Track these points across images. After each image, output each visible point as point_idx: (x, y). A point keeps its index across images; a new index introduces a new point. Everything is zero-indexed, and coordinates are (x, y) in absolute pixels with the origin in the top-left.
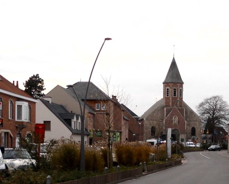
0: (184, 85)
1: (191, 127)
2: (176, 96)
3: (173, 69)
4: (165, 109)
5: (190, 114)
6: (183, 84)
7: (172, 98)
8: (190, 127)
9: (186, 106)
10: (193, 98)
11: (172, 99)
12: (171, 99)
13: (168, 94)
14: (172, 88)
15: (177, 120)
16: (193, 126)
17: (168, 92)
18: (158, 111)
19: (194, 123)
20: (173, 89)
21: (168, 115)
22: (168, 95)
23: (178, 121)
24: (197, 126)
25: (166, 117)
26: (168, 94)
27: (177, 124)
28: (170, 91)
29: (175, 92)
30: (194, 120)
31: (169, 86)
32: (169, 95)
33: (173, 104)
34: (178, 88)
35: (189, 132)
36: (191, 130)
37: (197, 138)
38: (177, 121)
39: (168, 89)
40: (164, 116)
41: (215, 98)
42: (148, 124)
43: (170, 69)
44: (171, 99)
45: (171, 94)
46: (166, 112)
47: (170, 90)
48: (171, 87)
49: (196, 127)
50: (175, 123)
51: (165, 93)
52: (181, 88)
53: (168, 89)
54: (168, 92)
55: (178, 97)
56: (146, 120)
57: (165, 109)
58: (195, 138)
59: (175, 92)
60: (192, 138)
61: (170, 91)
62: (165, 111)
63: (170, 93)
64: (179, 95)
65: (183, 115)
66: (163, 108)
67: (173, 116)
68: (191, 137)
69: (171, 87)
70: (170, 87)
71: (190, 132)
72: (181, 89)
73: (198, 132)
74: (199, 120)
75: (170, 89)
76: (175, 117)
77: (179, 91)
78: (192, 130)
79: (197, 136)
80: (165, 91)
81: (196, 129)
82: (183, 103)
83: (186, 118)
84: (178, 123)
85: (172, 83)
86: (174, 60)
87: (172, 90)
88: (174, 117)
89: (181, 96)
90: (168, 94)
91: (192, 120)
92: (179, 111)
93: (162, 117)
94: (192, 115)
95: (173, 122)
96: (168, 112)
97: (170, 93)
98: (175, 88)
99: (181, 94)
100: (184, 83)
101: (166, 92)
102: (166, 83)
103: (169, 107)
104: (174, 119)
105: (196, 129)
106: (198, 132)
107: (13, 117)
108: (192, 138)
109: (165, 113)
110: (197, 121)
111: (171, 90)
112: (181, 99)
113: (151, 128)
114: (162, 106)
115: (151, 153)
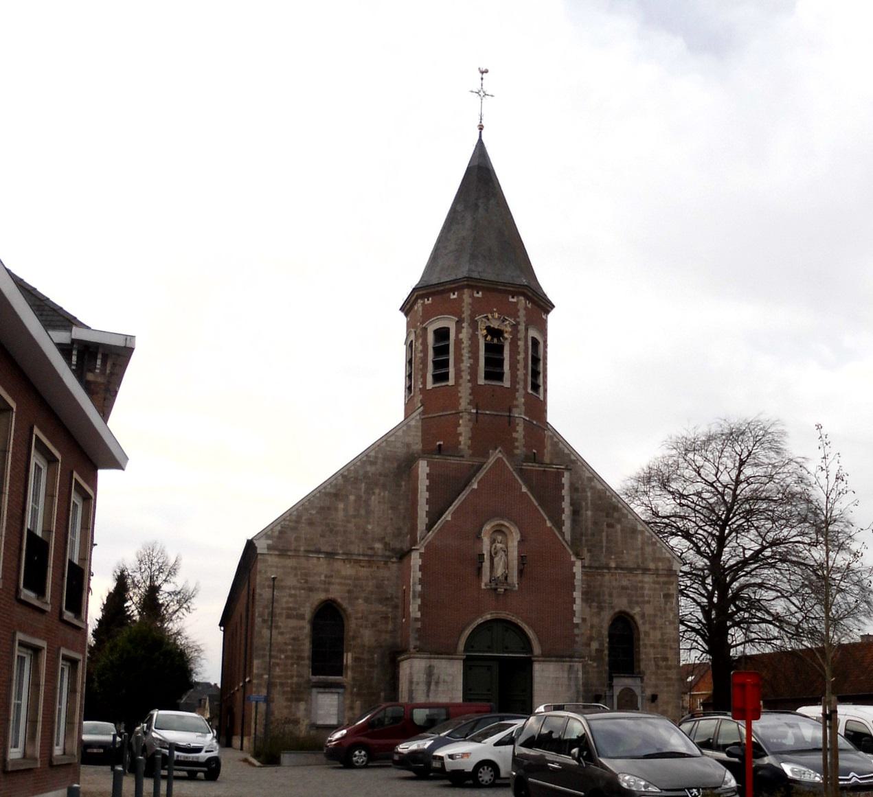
0: (552, 319)
1: (607, 616)
2: (507, 383)
3: (476, 206)
4: (423, 468)
5: (595, 523)
6: (547, 312)
7: (476, 390)
8: (601, 608)
9: (570, 461)
10: (619, 401)
11: (474, 403)
12: (464, 403)
13: (445, 364)
14: (474, 325)
15: (514, 553)
16: (621, 604)
17: (441, 350)
18: (370, 491)
19: (625, 582)
20: (482, 326)
21: (448, 516)
22: (445, 377)
23: (522, 559)
24: (649, 609)
25: (429, 527)
26: (441, 364)
27: (514, 578)
28: (458, 342)
29: (494, 350)
30: (630, 559)
31: (456, 311)
32: (452, 370)
33: (481, 446)
34: (515, 327)
35: (595, 645)
36: (605, 632)
37: (649, 692)
38: (514, 563)
39: (442, 334)
40: (414, 528)
41: (733, 436)
42: (291, 581)
43: (459, 208)
44: (464, 403)
45: (466, 364)
46: (429, 489)
47: (460, 336)
48: (466, 315)
49: (643, 616)
50: (499, 572)
51: (424, 361)
52: (533, 333)
53: (442, 334)
54: (441, 350)
55: (520, 386)
56: (269, 548)
57: (423, 468)
58: (638, 691)
59: (494, 350)
60: (617, 691)
61: (458, 342)
62: (423, 483)
63: (458, 360)
64: (523, 373)
65: (559, 524)
66: (406, 467)
67: (488, 519)
68: (611, 686)
69: (466, 315)
70: (457, 313)
71: (599, 651)
72: (535, 343)
73: (653, 646)
74: (656, 560)
75: (458, 331)
76: (499, 530)
77: (521, 343)
78: (611, 636)
79: (650, 679)
80: (425, 351)
81: (642, 628)
82: (548, 443)
83: (576, 543)
84: (521, 572)
85: (471, 283)
86: (480, 151)
87: (473, 338)
88: (487, 528)
89: (535, 387)
90: (441, 364)
91: (613, 565)
92: (524, 489)
93: (398, 534)
94: (610, 526)
95: (486, 564)
96: (445, 490)
97: (458, 360)
98: (495, 324)
99: (535, 374)
100: (553, 306)
101: (430, 361)
102: (424, 301)
103: (452, 460)
104: (493, 541)
105: (643, 627)
106: (653, 646)
107: (176, 770)
108: (617, 691)
109: (423, 495)
110: (645, 570)
111: (465, 335)
112: (538, 407)
113: (308, 611)
114: (401, 451)
115: (693, 677)
